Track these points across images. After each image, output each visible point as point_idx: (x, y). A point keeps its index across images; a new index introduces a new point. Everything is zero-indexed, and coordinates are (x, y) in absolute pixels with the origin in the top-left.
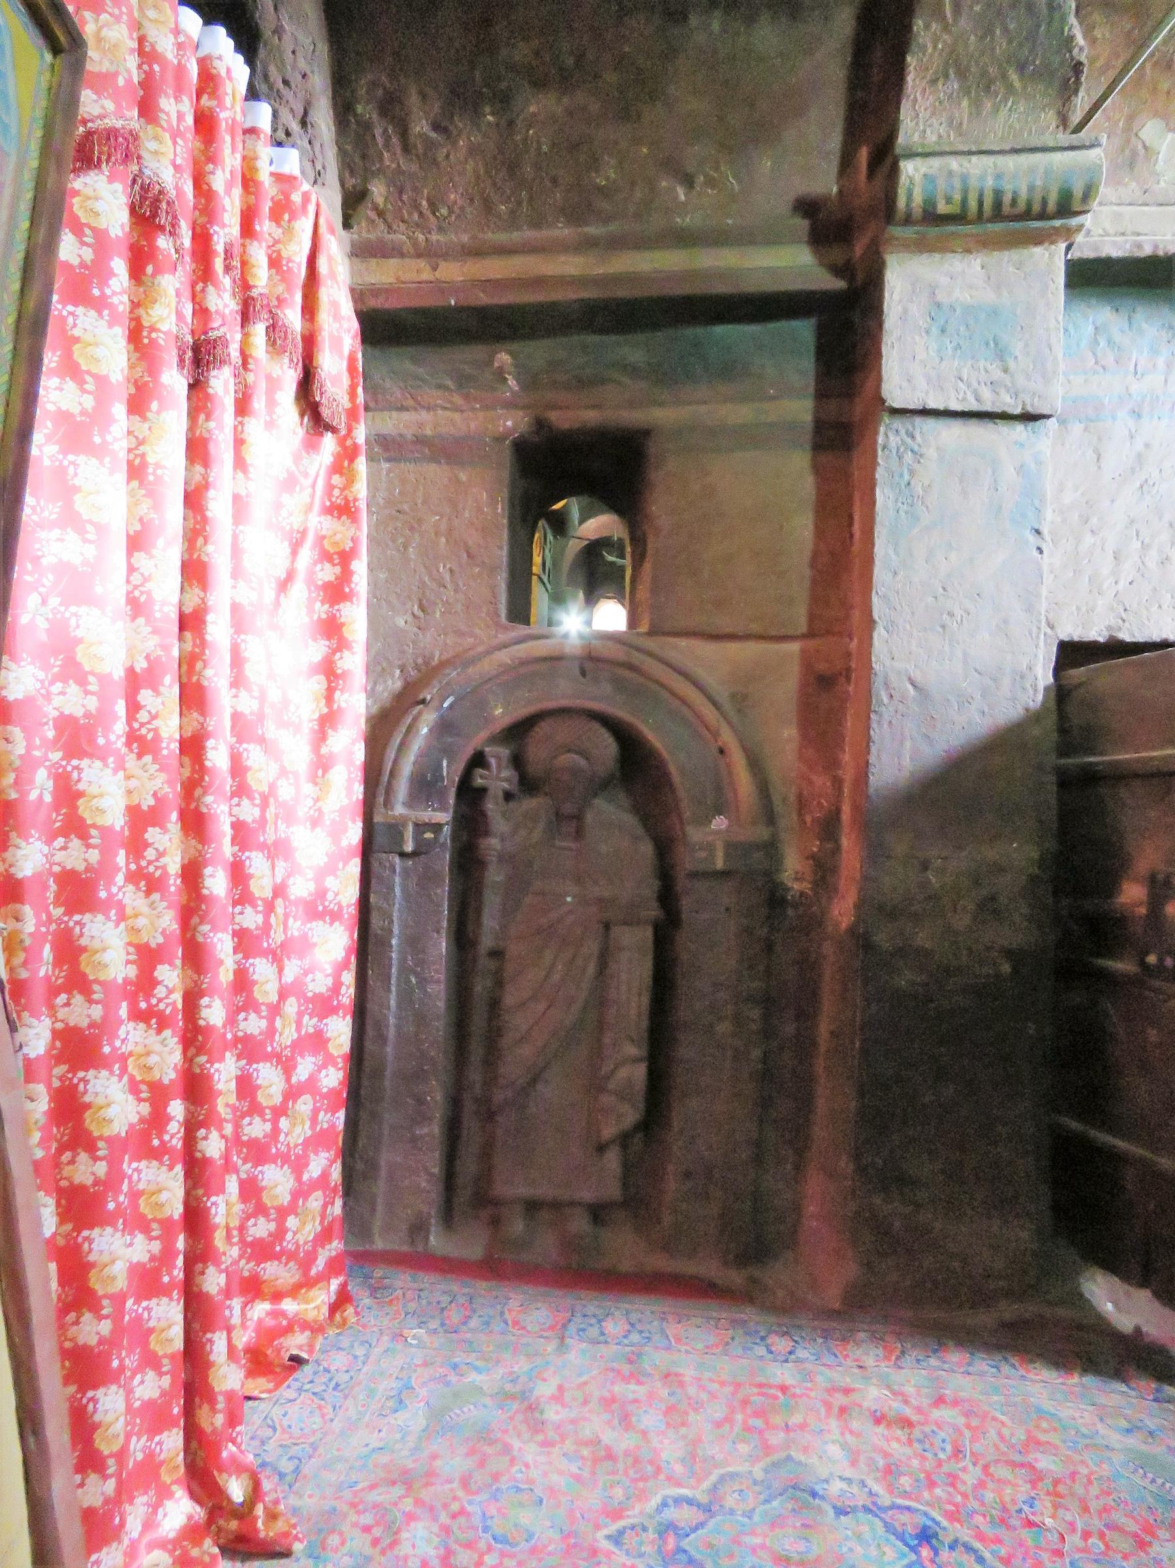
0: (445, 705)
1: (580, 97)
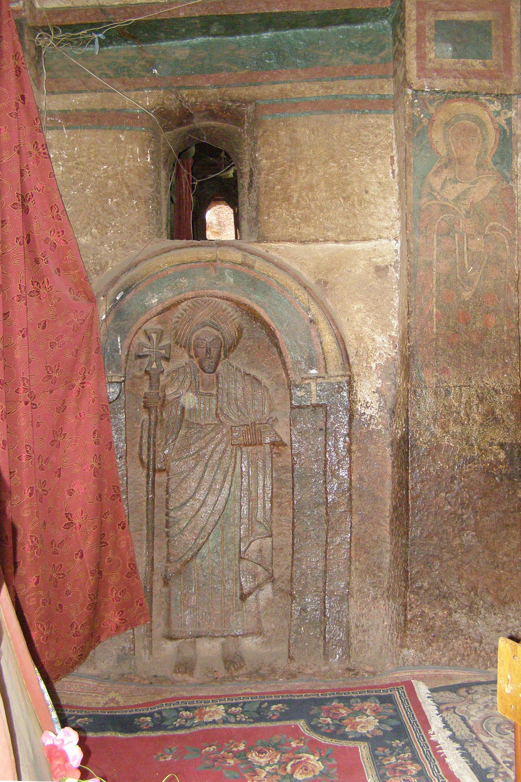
0: (118, 298)
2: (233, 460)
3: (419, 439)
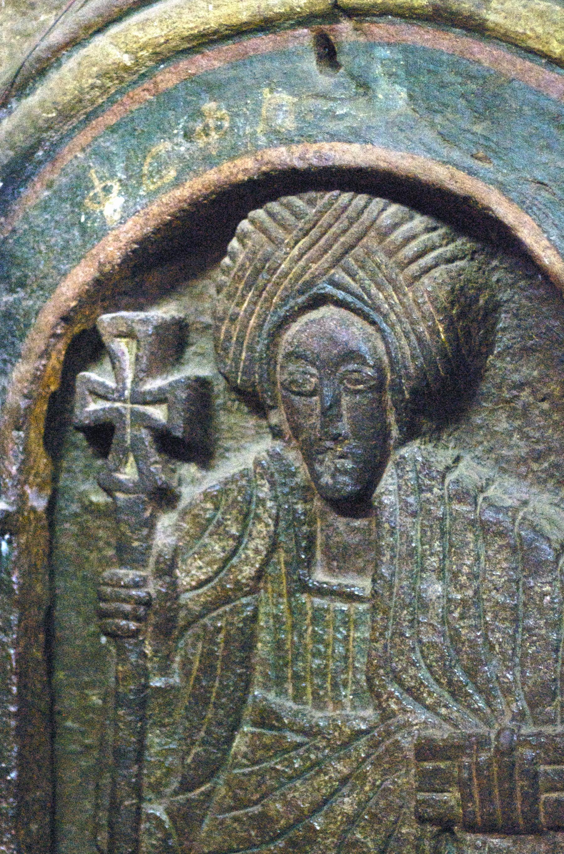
1: (115, 136)
2: (301, 300)
3: (460, 571)
